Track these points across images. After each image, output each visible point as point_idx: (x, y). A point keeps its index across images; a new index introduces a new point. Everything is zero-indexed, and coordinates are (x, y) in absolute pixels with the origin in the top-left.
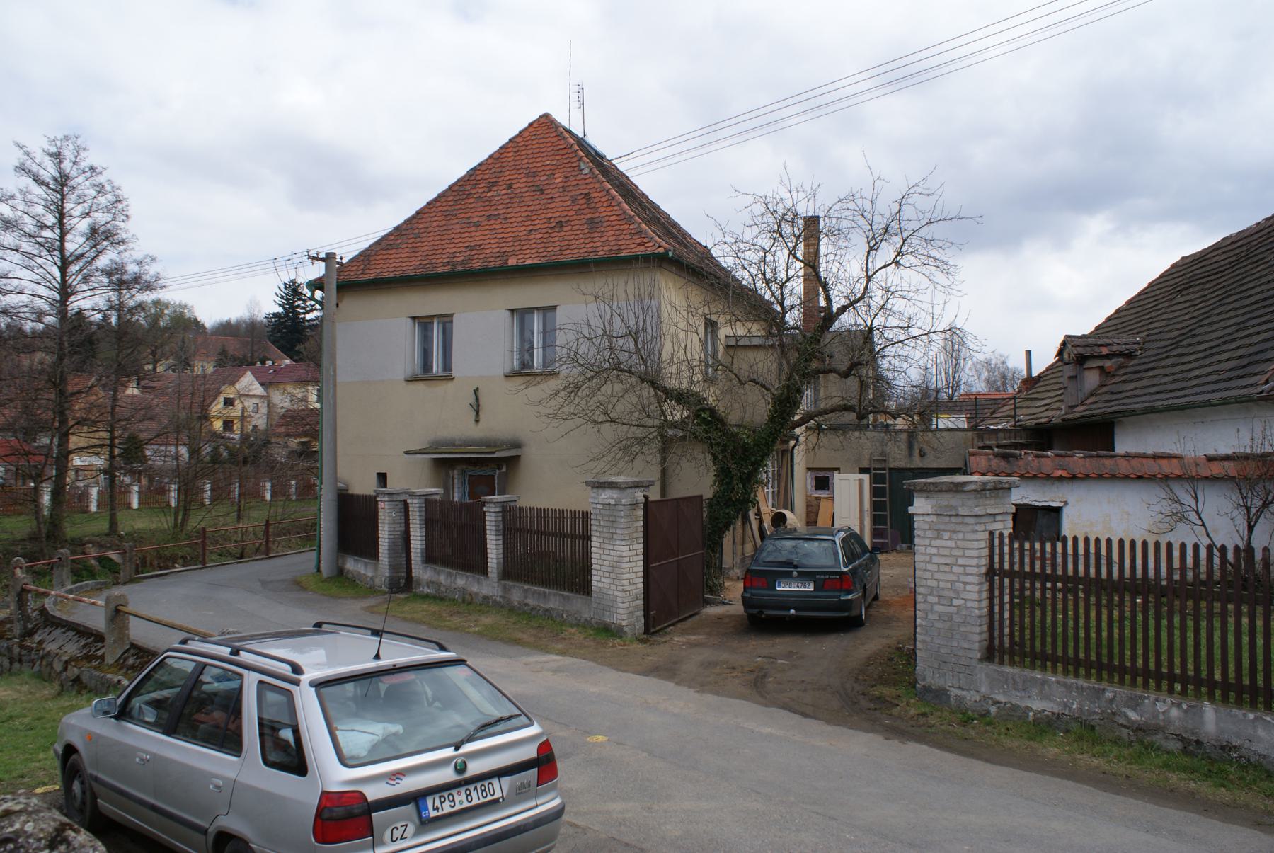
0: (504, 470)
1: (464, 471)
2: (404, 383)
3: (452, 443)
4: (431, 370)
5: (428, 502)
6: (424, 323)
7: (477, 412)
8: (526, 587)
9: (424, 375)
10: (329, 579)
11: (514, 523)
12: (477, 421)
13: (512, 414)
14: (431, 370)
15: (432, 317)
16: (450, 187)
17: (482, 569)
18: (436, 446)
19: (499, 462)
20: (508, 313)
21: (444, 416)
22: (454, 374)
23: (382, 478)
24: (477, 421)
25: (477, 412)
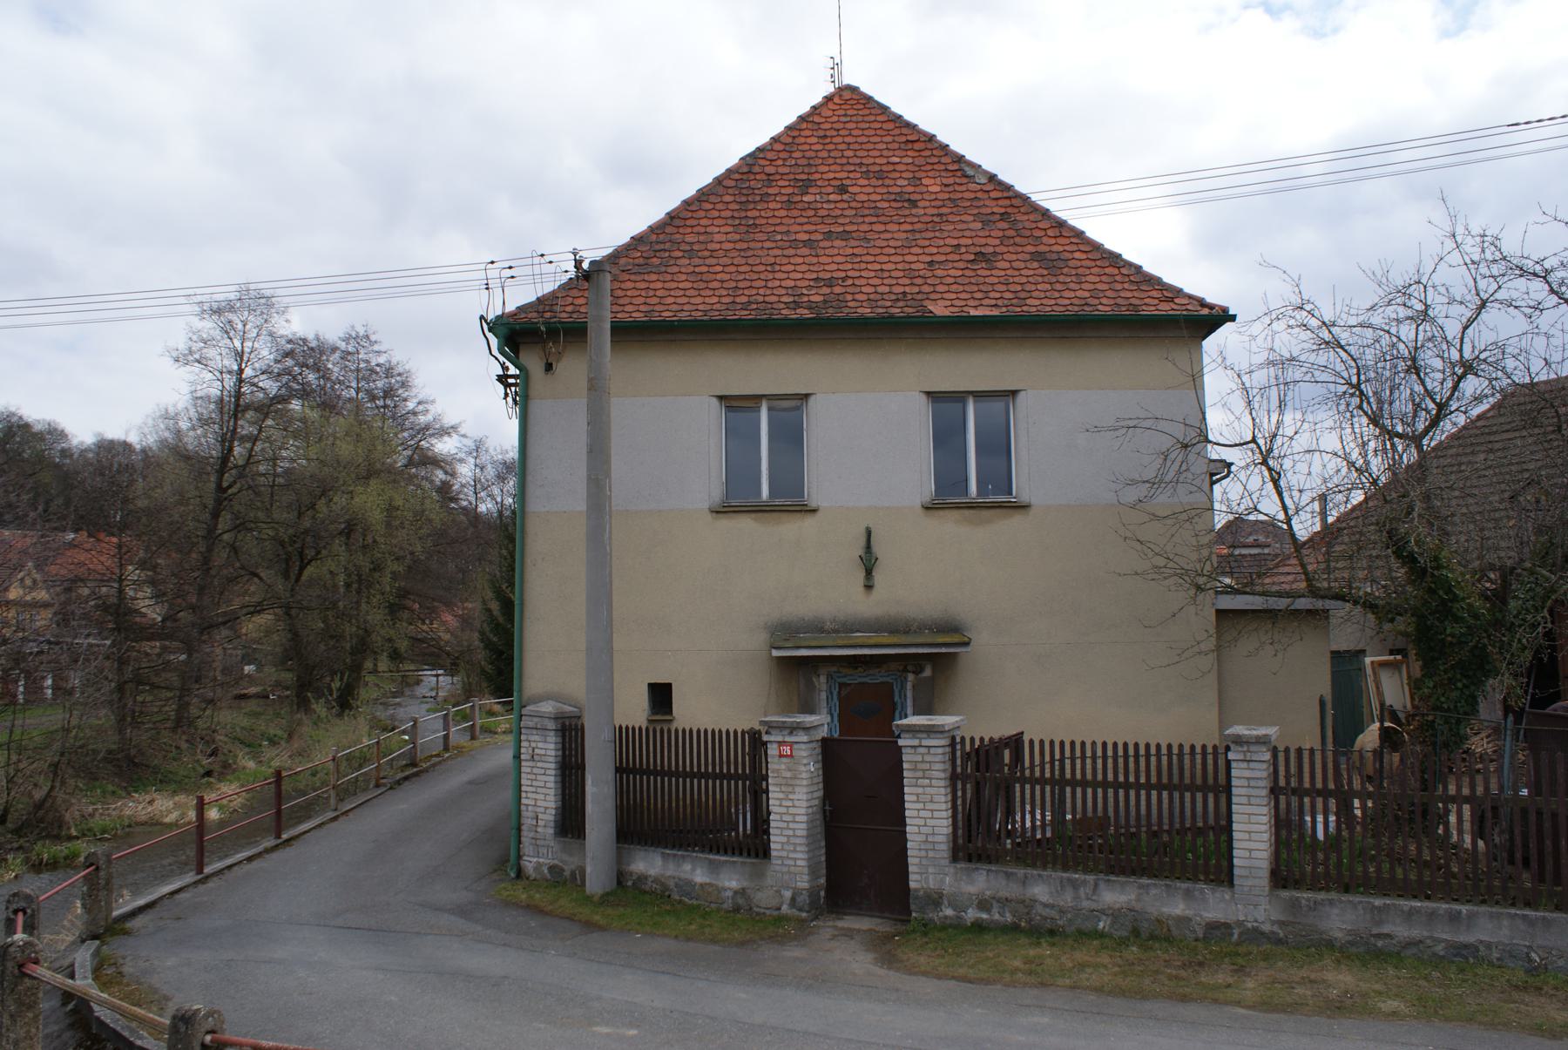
0: (928, 672)
1: (830, 677)
2: (709, 517)
3: (817, 628)
4: (766, 486)
5: (624, 737)
6: (736, 405)
7: (869, 573)
8: (1378, 902)
9: (736, 502)
10: (605, 900)
11: (987, 773)
12: (869, 587)
13: (937, 570)
14: (766, 486)
15: (758, 398)
16: (718, 181)
17: (1222, 874)
18: (784, 631)
19: (912, 663)
20: (924, 397)
21: (801, 577)
22: (1022, 486)
23: (661, 696)
24: (869, 587)
25: (869, 573)
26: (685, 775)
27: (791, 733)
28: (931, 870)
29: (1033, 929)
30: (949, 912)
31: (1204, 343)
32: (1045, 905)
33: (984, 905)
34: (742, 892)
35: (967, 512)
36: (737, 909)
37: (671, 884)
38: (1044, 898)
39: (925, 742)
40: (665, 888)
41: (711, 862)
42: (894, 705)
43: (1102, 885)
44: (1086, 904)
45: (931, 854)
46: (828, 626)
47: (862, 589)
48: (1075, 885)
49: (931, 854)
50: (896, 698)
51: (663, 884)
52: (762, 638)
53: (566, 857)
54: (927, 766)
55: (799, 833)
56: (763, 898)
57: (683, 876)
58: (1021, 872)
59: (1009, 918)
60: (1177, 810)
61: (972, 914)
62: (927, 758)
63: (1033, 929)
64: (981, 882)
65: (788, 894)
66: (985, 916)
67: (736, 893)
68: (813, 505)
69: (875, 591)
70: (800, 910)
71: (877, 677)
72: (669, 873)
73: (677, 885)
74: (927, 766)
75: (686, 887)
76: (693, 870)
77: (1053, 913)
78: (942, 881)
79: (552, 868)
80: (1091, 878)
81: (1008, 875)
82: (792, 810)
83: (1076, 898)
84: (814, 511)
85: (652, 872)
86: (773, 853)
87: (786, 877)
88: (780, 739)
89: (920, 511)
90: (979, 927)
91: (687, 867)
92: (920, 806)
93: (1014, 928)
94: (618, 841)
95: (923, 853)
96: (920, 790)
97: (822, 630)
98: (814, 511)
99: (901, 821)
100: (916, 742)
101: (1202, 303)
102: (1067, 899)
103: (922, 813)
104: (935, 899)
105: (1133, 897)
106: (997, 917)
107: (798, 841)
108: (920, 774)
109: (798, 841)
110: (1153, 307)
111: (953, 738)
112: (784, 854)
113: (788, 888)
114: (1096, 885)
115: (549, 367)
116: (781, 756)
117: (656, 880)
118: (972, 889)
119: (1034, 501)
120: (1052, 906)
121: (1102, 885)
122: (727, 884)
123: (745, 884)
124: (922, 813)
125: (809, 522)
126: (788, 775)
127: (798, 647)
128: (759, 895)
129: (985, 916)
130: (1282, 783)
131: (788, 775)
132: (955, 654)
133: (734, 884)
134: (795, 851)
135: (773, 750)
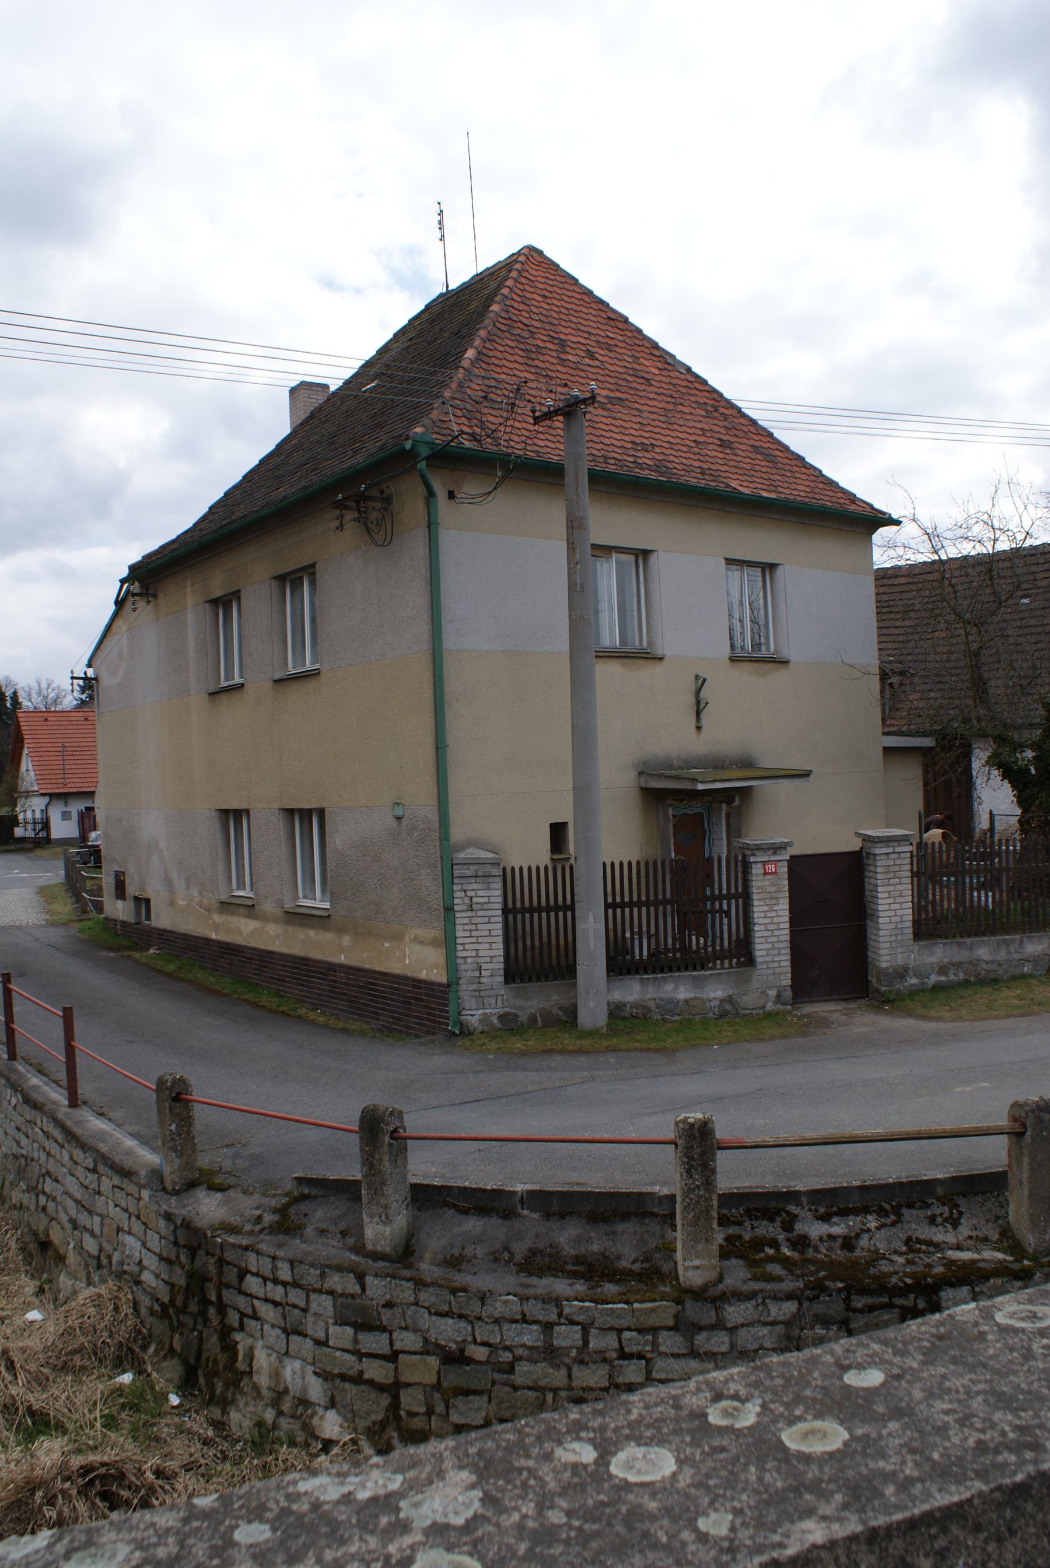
21: (643, 722)
25: (698, 713)
26: (539, 910)
27: (775, 853)
28: (899, 950)
29: (989, 981)
30: (914, 981)
31: (874, 536)
32: (987, 962)
33: (943, 970)
34: (730, 999)
35: (755, 665)
36: (724, 1014)
37: (652, 1005)
38: (986, 957)
39: (898, 850)
40: (648, 1010)
41: (694, 977)
42: (704, 831)
43: (1025, 940)
44: (1015, 956)
45: (899, 938)
46: (676, 763)
47: (694, 730)
48: (1007, 943)
49: (899, 938)
50: (706, 826)
51: (644, 1007)
52: (632, 774)
53: (518, 1002)
54: (898, 868)
55: (782, 938)
56: (749, 1000)
57: (664, 996)
58: (969, 940)
59: (962, 976)
60: (536, 927)
61: (934, 979)
62: (898, 862)
63: (989, 981)
64: (940, 953)
65: (773, 993)
66: (943, 978)
67: (722, 1001)
68: (660, 654)
69: (704, 729)
70: (783, 1004)
71: (696, 808)
72: (649, 996)
73: (658, 1006)
74: (898, 868)
75: (668, 1007)
76: (676, 988)
77: (994, 967)
78: (909, 958)
79: (502, 1017)
80: (1017, 937)
81: (959, 944)
82: (776, 920)
83: (1008, 953)
84: (661, 659)
85: (630, 998)
86: (759, 960)
87: (771, 978)
88: (766, 858)
89: (728, 662)
90: (938, 988)
91: (669, 987)
92: (891, 901)
93: (965, 984)
94: (608, 975)
95: (893, 938)
96: (892, 888)
97: (671, 767)
98: (661, 659)
99: (793, 922)
100: (890, 850)
101: (852, 498)
102: (1002, 955)
103: (893, 907)
104: (901, 973)
105: (1046, 945)
106: (952, 977)
107: (782, 945)
108: (892, 875)
109: (782, 945)
110: (825, 500)
111: (504, 869)
112: (769, 958)
113: (771, 988)
114: (1021, 941)
115: (451, 495)
116: (765, 873)
117: (636, 1005)
118: (933, 959)
119: (792, 658)
120: (992, 962)
121: (1025, 940)
122: (712, 995)
123: (731, 992)
124: (893, 907)
125: (659, 668)
126: (773, 889)
127: (715, 781)
128: (745, 999)
129: (943, 978)
130: (510, 905)
131: (773, 889)
132: (750, 788)
133: (720, 994)
134: (779, 954)
135: (757, 870)
